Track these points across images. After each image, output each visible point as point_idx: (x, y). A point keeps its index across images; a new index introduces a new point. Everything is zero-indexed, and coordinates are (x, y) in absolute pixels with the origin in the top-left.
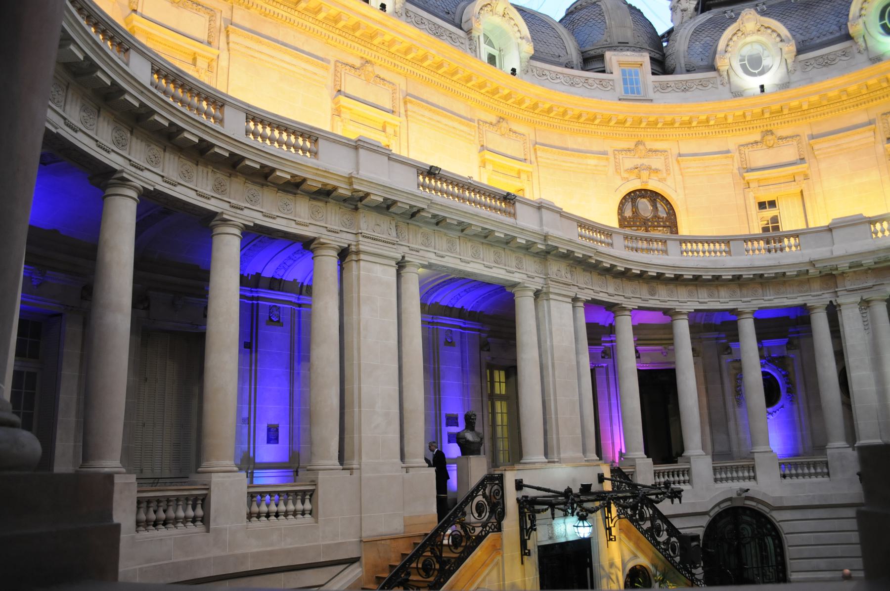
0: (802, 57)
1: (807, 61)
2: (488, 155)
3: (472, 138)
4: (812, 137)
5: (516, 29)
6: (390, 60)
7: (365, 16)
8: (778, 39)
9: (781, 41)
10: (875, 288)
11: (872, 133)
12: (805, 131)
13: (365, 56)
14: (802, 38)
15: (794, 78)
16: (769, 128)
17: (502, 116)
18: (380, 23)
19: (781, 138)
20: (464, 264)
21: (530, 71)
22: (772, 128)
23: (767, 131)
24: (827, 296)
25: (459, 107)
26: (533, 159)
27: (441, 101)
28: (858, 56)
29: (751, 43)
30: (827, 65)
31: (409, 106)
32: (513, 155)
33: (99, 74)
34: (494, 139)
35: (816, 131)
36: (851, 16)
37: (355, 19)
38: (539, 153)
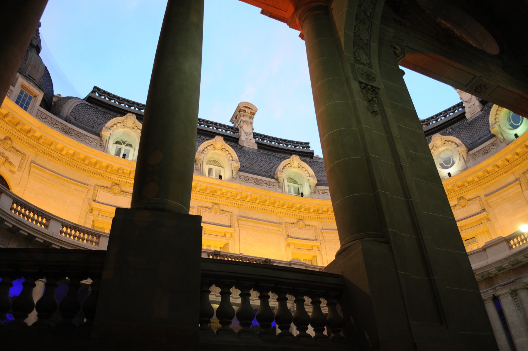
0: (471, 152)
1: (474, 154)
2: (290, 240)
3: (280, 233)
4: (487, 195)
5: (307, 172)
6: (228, 201)
7: (209, 183)
8: (456, 146)
9: (458, 146)
10: (517, 281)
11: (519, 186)
12: (482, 193)
13: (214, 201)
14: (471, 142)
15: (469, 165)
16: (461, 196)
17: (300, 218)
18: (218, 185)
19: (469, 200)
20: (235, 299)
21: (317, 192)
22: (462, 195)
23: (460, 198)
24: (490, 291)
25: (274, 219)
26: (321, 238)
27: (260, 216)
28: (501, 144)
29: (443, 151)
30: (485, 153)
31: (240, 222)
32: (308, 238)
33: (21, 231)
34: (295, 231)
35: (488, 191)
36: (490, 124)
37: (205, 185)
38: (324, 235)
